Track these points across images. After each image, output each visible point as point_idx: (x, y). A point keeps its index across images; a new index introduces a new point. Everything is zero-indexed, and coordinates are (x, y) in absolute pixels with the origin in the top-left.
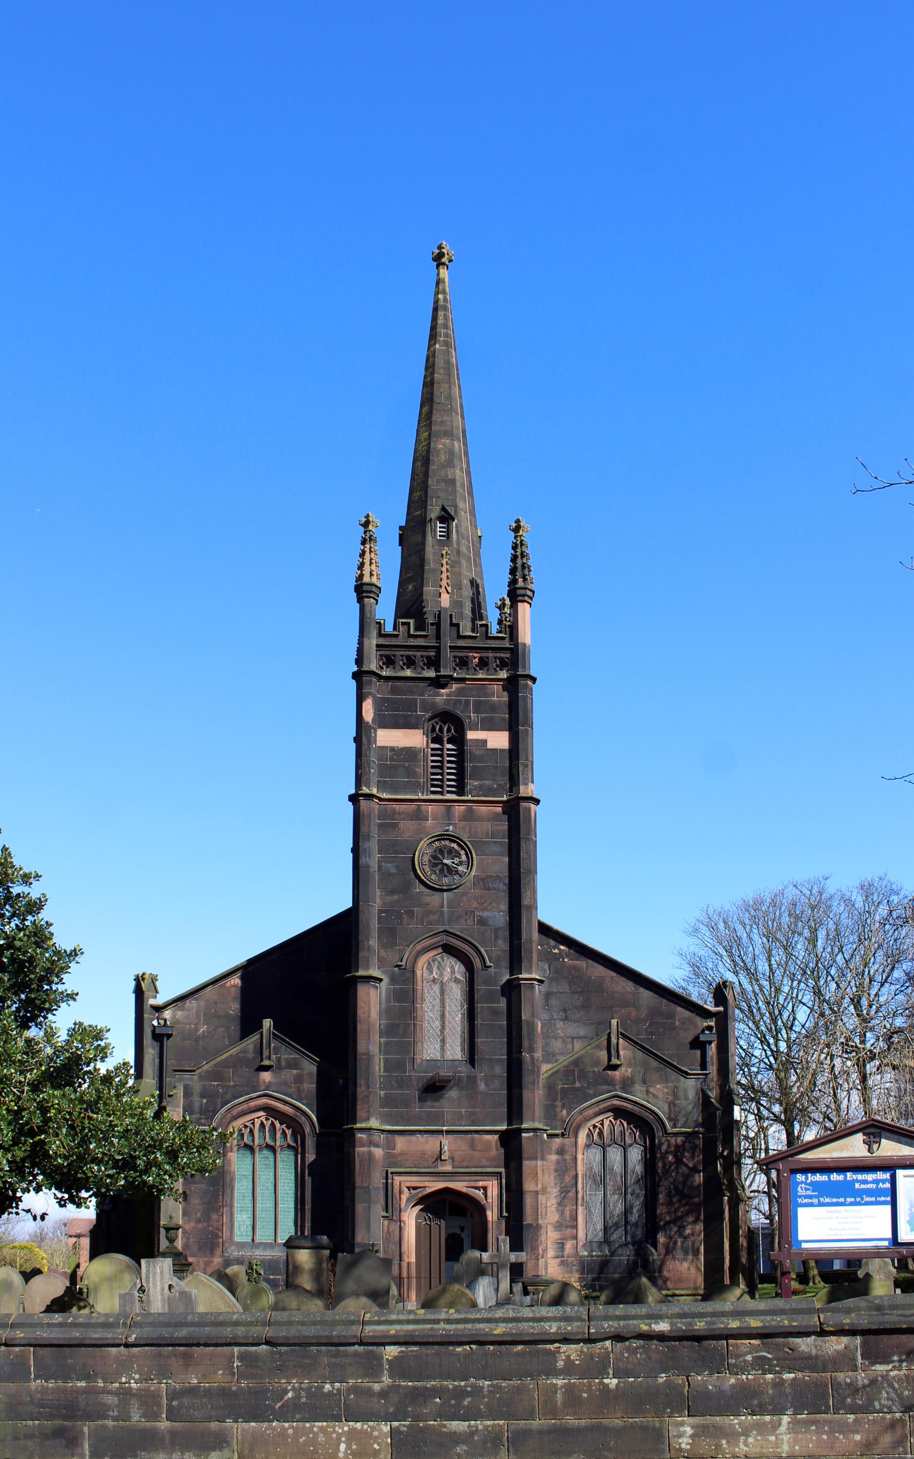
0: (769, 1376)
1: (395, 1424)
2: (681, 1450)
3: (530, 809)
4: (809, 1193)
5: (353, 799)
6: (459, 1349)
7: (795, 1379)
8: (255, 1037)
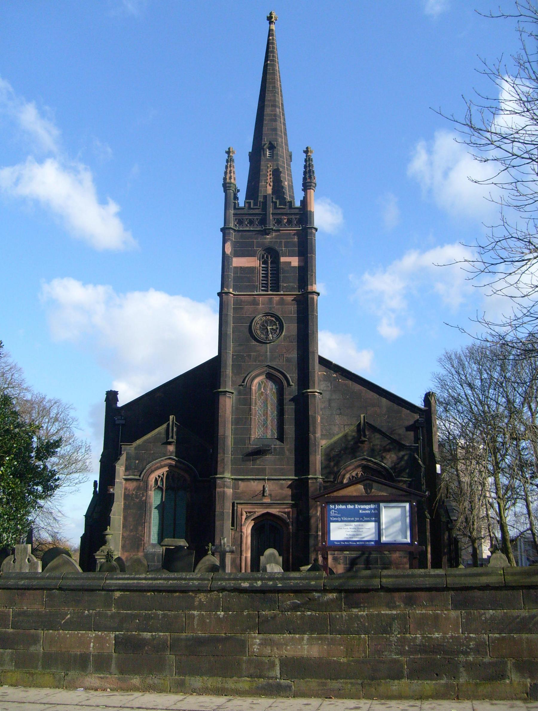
0: (299, 613)
1: (117, 633)
2: (254, 652)
3: (313, 298)
4: (336, 515)
5: (219, 294)
6: (149, 594)
7: (311, 615)
8: (165, 426)
